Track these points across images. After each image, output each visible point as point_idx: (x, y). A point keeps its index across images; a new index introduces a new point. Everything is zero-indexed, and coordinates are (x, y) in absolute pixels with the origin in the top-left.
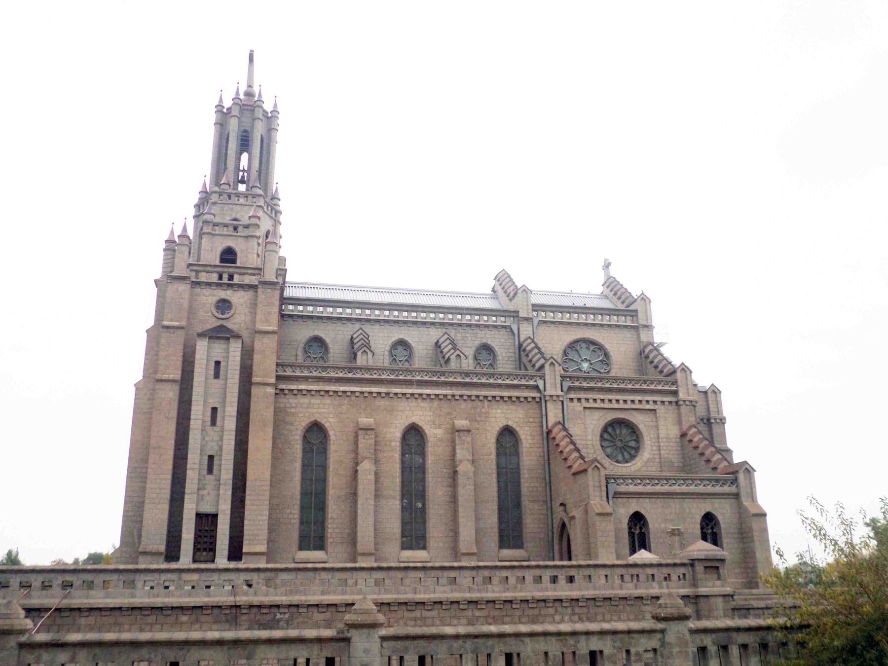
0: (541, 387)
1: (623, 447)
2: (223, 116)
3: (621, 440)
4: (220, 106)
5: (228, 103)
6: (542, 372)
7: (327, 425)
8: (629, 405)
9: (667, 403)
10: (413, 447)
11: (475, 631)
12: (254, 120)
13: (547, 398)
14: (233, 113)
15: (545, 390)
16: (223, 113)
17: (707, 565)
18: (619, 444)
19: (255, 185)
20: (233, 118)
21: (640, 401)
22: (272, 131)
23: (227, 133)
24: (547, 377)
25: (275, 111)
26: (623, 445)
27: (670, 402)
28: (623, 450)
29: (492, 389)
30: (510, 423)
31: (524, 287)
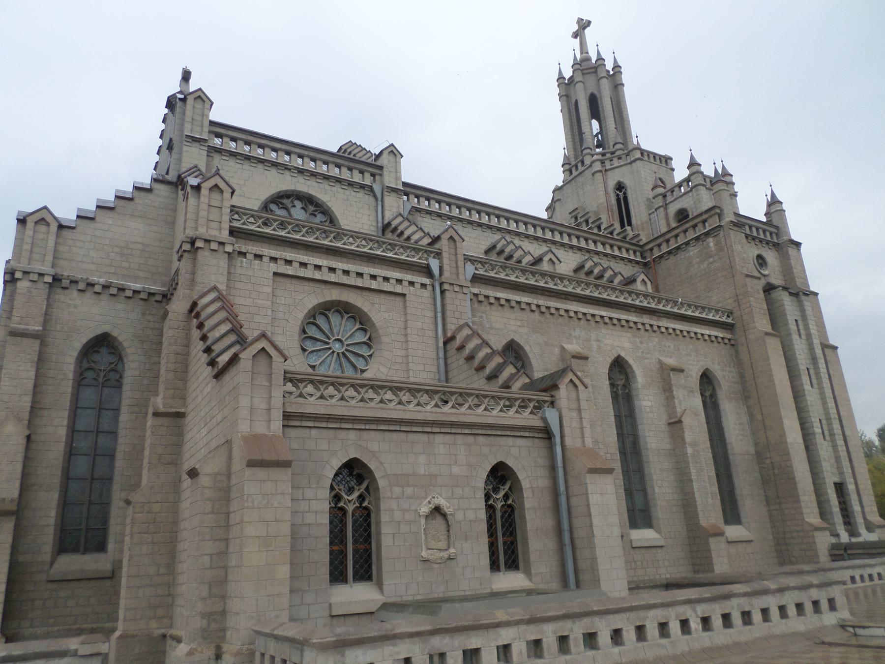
0: (436, 271)
1: (343, 353)
2: (566, 87)
3: (339, 340)
4: (561, 77)
5: (568, 73)
6: (437, 246)
8: (352, 280)
9: (418, 286)
10: (619, 388)
11: (625, 641)
12: (599, 80)
13: (446, 287)
14: (577, 80)
15: (441, 274)
16: (566, 84)
18: (337, 347)
19: (618, 141)
20: (578, 84)
21: (399, 281)
22: (619, 87)
23: (573, 102)
24: (445, 255)
25: (617, 66)
26: (345, 347)
27: (423, 286)
28: (343, 360)
29: (286, 248)
31: (199, 93)
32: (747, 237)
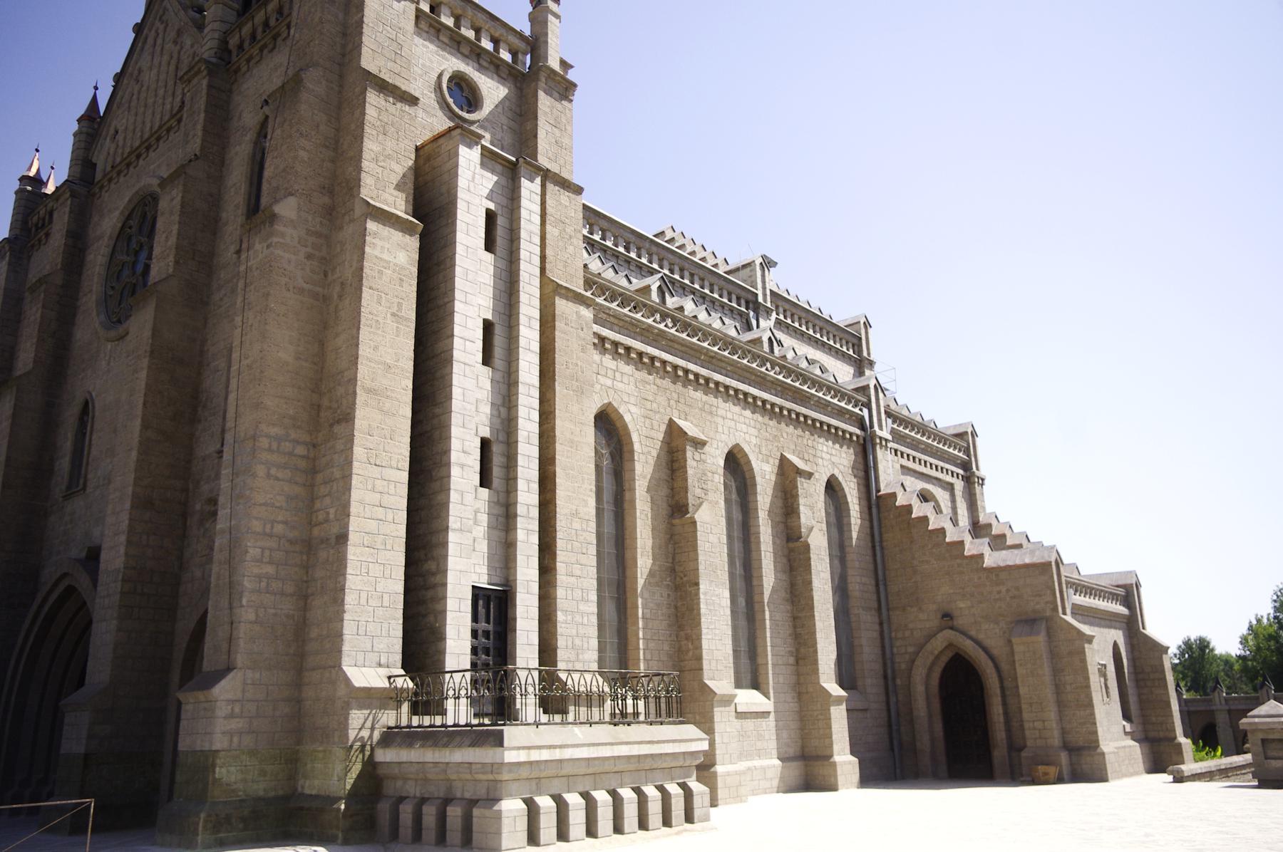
7: (627, 418)
17: (910, 464)
30: (836, 473)
32: (417, 17)
